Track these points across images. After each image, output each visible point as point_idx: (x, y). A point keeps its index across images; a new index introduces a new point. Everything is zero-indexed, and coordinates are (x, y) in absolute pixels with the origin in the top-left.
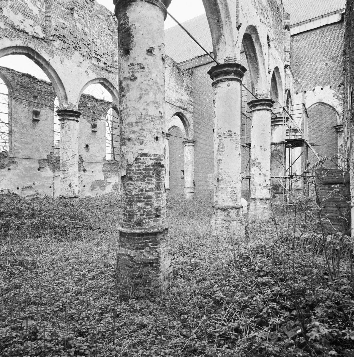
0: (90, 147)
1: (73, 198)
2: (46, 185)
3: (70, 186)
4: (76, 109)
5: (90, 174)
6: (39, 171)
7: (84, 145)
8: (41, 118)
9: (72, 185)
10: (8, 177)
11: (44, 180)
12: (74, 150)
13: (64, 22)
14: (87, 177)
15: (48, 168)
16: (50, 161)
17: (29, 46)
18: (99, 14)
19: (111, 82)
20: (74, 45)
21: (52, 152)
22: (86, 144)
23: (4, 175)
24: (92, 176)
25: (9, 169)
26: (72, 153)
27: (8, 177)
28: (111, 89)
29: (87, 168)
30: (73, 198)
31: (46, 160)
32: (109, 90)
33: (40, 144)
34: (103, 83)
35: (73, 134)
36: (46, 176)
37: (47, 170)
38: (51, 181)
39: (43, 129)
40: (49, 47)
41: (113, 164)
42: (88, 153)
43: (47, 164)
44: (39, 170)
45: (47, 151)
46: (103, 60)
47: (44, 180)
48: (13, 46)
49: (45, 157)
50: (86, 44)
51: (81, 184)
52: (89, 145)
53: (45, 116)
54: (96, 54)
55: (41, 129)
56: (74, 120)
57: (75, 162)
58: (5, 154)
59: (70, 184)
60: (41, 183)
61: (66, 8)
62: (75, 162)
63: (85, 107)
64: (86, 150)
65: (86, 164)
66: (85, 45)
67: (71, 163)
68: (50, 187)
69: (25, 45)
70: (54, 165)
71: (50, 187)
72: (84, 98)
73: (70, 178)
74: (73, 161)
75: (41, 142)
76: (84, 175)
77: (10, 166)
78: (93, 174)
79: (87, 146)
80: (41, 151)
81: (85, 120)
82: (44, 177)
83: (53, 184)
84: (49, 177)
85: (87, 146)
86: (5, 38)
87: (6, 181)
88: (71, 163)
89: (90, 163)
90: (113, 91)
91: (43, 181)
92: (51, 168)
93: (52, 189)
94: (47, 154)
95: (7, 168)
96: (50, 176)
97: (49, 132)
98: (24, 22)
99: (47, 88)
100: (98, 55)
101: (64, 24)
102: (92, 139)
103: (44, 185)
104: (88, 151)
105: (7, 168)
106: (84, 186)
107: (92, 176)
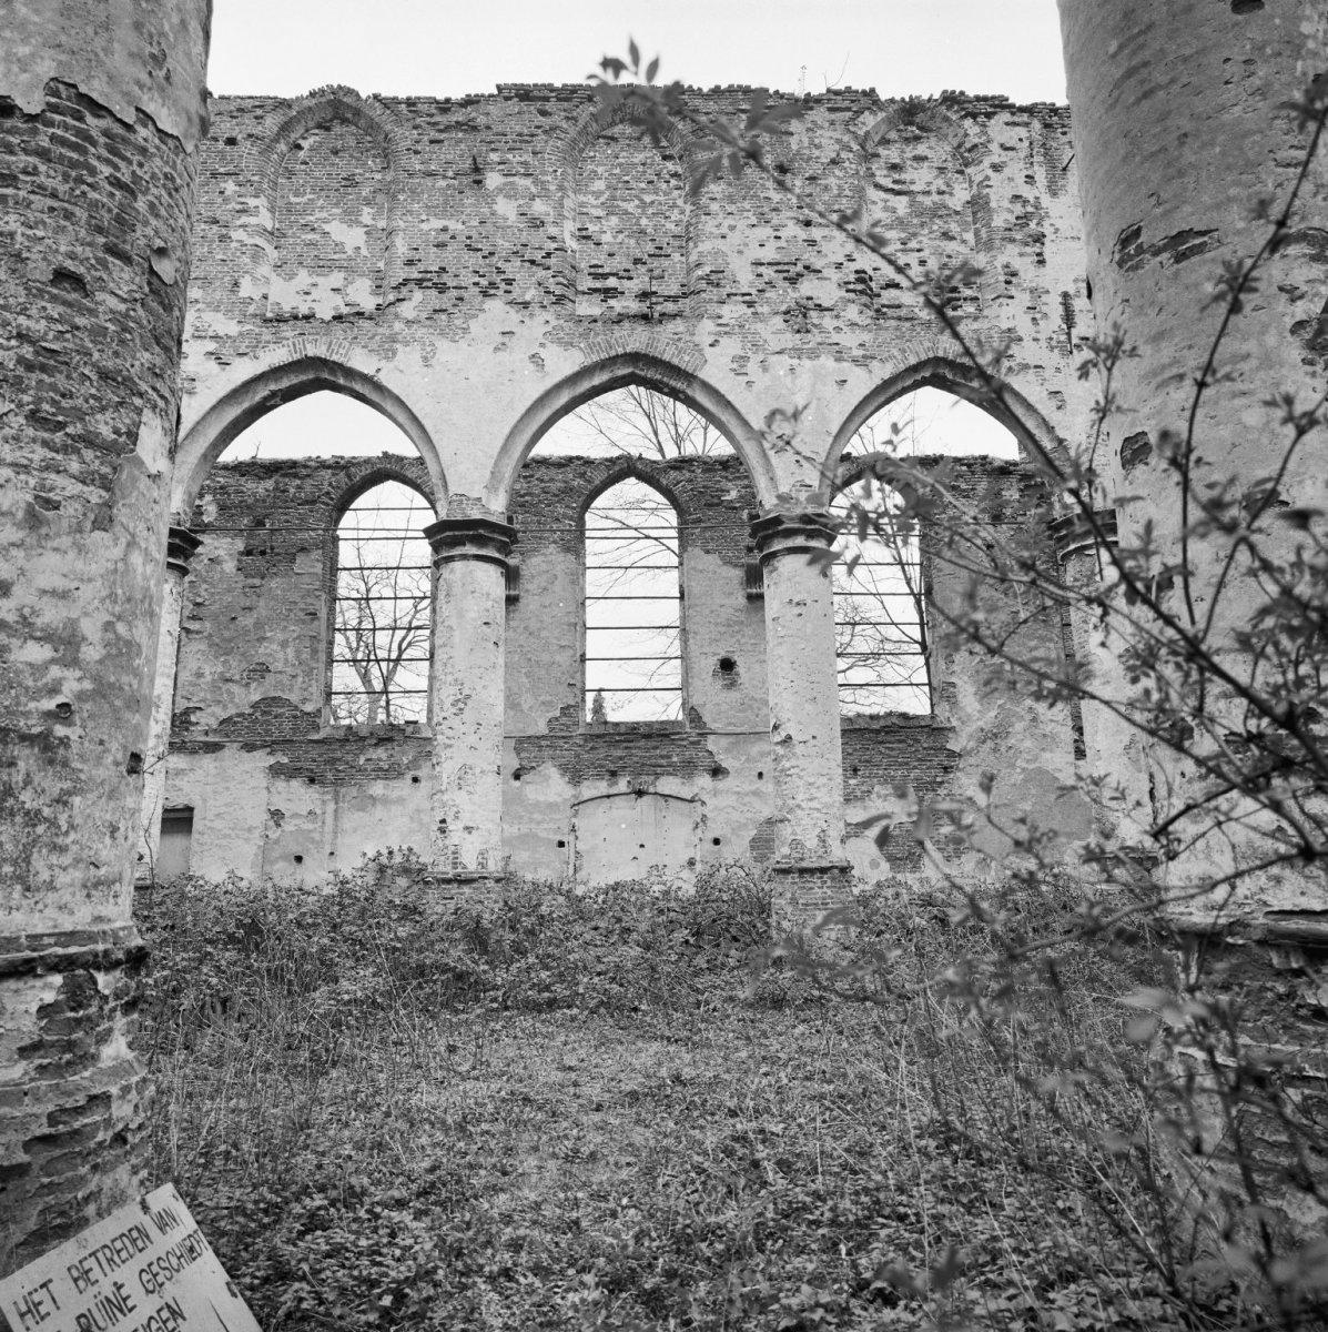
0: (741, 668)
1: (449, 881)
2: (543, 834)
3: (443, 831)
4: (496, 507)
5: (747, 787)
6: (517, 783)
7: (712, 663)
8: (529, 587)
9: (451, 826)
10: (411, 806)
11: (537, 816)
12: (460, 676)
13: (439, 224)
14: (722, 801)
15: (551, 771)
16: (561, 742)
17: (310, 354)
18: (613, 124)
19: (666, 357)
20: (484, 282)
21: (569, 707)
22: (723, 654)
23: (401, 801)
24: (756, 793)
25: (415, 780)
26: (453, 690)
27: (411, 806)
28: (679, 385)
29: (726, 762)
30: (449, 881)
31: (544, 737)
32: (675, 394)
33: (525, 680)
34: (632, 374)
35: (461, 615)
36: (542, 798)
37: (547, 778)
38: (563, 818)
39: (533, 625)
40: (380, 330)
41: (877, 732)
42: (734, 695)
43: (547, 753)
44: (517, 777)
45: (551, 702)
46: (634, 286)
47: (537, 816)
48: (259, 372)
49: (541, 728)
50: (538, 256)
51: (699, 831)
52: (735, 658)
53: (545, 577)
54: (596, 276)
55: (526, 628)
56: (464, 557)
57: (463, 729)
58: (410, 729)
59: (443, 821)
60: (524, 830)
61: (457, 175)
62: (463, 729)
63: (710, 505)
64: (719, 683)
65: (724, 741)
66: (533, 262)
67: (450, 733)
68: (561, 844)
69: (297, 357)
70: (577, 756)
71: (561, 844)
72: (704, 471)
73: (445, 798)
74: (455, 722)
75: (527, 675)
76: (715, 793)
77: (419, 768)
78: (759, 784)
79: (727, 665)
80: (525, 707)
81: (713, 559)
82: (537, 804)
83: (573, 829)
84: (556, 804)
85: (727, 665)
86: (238, 360)
87: (406, 820)
88: (450, 733)
89: (740, 737)
90: (689, 392)
91: (531, 820)
92: (564, 769)
93: (568, 851)
94: (550, 715)
95: (409, 777)
96: (559, 800)
97: (556, 634)
98: (313, 290)
99: (552, 480)
100: (605, 276)
101: (445, 229)
102: (748, 631)
103: (535, 836)
104: (732, 685)
105: (409, 777)
106: (717, 842)
107: (756, 793)
